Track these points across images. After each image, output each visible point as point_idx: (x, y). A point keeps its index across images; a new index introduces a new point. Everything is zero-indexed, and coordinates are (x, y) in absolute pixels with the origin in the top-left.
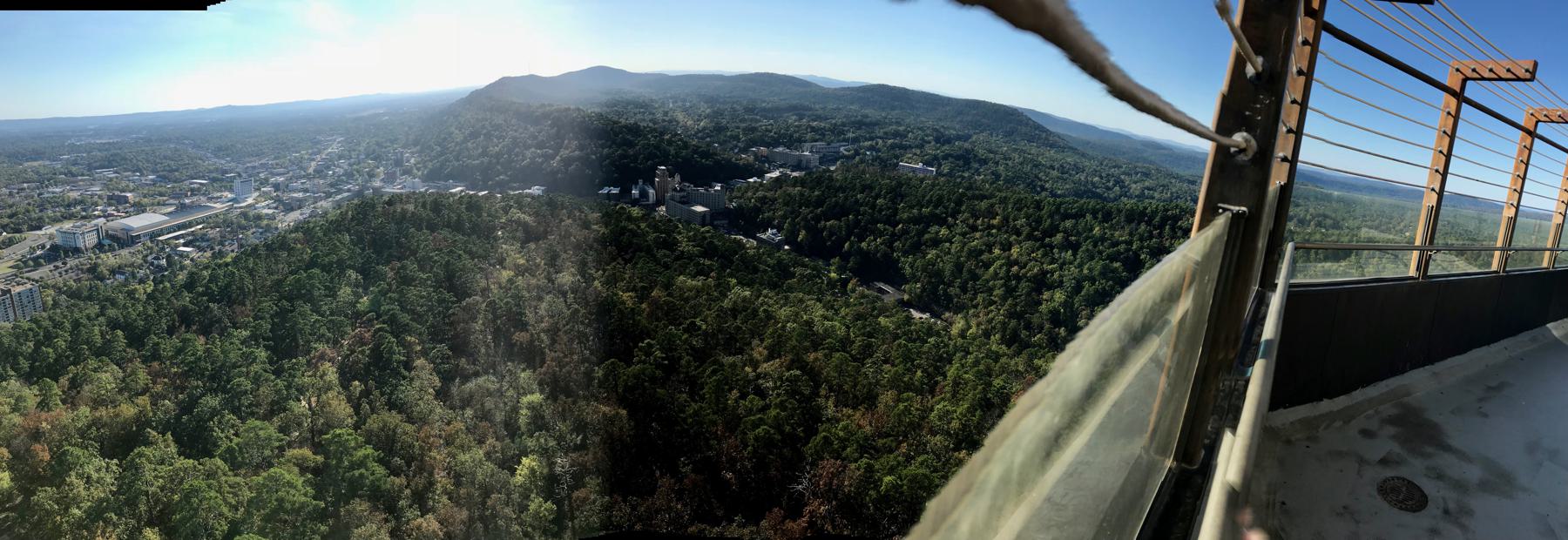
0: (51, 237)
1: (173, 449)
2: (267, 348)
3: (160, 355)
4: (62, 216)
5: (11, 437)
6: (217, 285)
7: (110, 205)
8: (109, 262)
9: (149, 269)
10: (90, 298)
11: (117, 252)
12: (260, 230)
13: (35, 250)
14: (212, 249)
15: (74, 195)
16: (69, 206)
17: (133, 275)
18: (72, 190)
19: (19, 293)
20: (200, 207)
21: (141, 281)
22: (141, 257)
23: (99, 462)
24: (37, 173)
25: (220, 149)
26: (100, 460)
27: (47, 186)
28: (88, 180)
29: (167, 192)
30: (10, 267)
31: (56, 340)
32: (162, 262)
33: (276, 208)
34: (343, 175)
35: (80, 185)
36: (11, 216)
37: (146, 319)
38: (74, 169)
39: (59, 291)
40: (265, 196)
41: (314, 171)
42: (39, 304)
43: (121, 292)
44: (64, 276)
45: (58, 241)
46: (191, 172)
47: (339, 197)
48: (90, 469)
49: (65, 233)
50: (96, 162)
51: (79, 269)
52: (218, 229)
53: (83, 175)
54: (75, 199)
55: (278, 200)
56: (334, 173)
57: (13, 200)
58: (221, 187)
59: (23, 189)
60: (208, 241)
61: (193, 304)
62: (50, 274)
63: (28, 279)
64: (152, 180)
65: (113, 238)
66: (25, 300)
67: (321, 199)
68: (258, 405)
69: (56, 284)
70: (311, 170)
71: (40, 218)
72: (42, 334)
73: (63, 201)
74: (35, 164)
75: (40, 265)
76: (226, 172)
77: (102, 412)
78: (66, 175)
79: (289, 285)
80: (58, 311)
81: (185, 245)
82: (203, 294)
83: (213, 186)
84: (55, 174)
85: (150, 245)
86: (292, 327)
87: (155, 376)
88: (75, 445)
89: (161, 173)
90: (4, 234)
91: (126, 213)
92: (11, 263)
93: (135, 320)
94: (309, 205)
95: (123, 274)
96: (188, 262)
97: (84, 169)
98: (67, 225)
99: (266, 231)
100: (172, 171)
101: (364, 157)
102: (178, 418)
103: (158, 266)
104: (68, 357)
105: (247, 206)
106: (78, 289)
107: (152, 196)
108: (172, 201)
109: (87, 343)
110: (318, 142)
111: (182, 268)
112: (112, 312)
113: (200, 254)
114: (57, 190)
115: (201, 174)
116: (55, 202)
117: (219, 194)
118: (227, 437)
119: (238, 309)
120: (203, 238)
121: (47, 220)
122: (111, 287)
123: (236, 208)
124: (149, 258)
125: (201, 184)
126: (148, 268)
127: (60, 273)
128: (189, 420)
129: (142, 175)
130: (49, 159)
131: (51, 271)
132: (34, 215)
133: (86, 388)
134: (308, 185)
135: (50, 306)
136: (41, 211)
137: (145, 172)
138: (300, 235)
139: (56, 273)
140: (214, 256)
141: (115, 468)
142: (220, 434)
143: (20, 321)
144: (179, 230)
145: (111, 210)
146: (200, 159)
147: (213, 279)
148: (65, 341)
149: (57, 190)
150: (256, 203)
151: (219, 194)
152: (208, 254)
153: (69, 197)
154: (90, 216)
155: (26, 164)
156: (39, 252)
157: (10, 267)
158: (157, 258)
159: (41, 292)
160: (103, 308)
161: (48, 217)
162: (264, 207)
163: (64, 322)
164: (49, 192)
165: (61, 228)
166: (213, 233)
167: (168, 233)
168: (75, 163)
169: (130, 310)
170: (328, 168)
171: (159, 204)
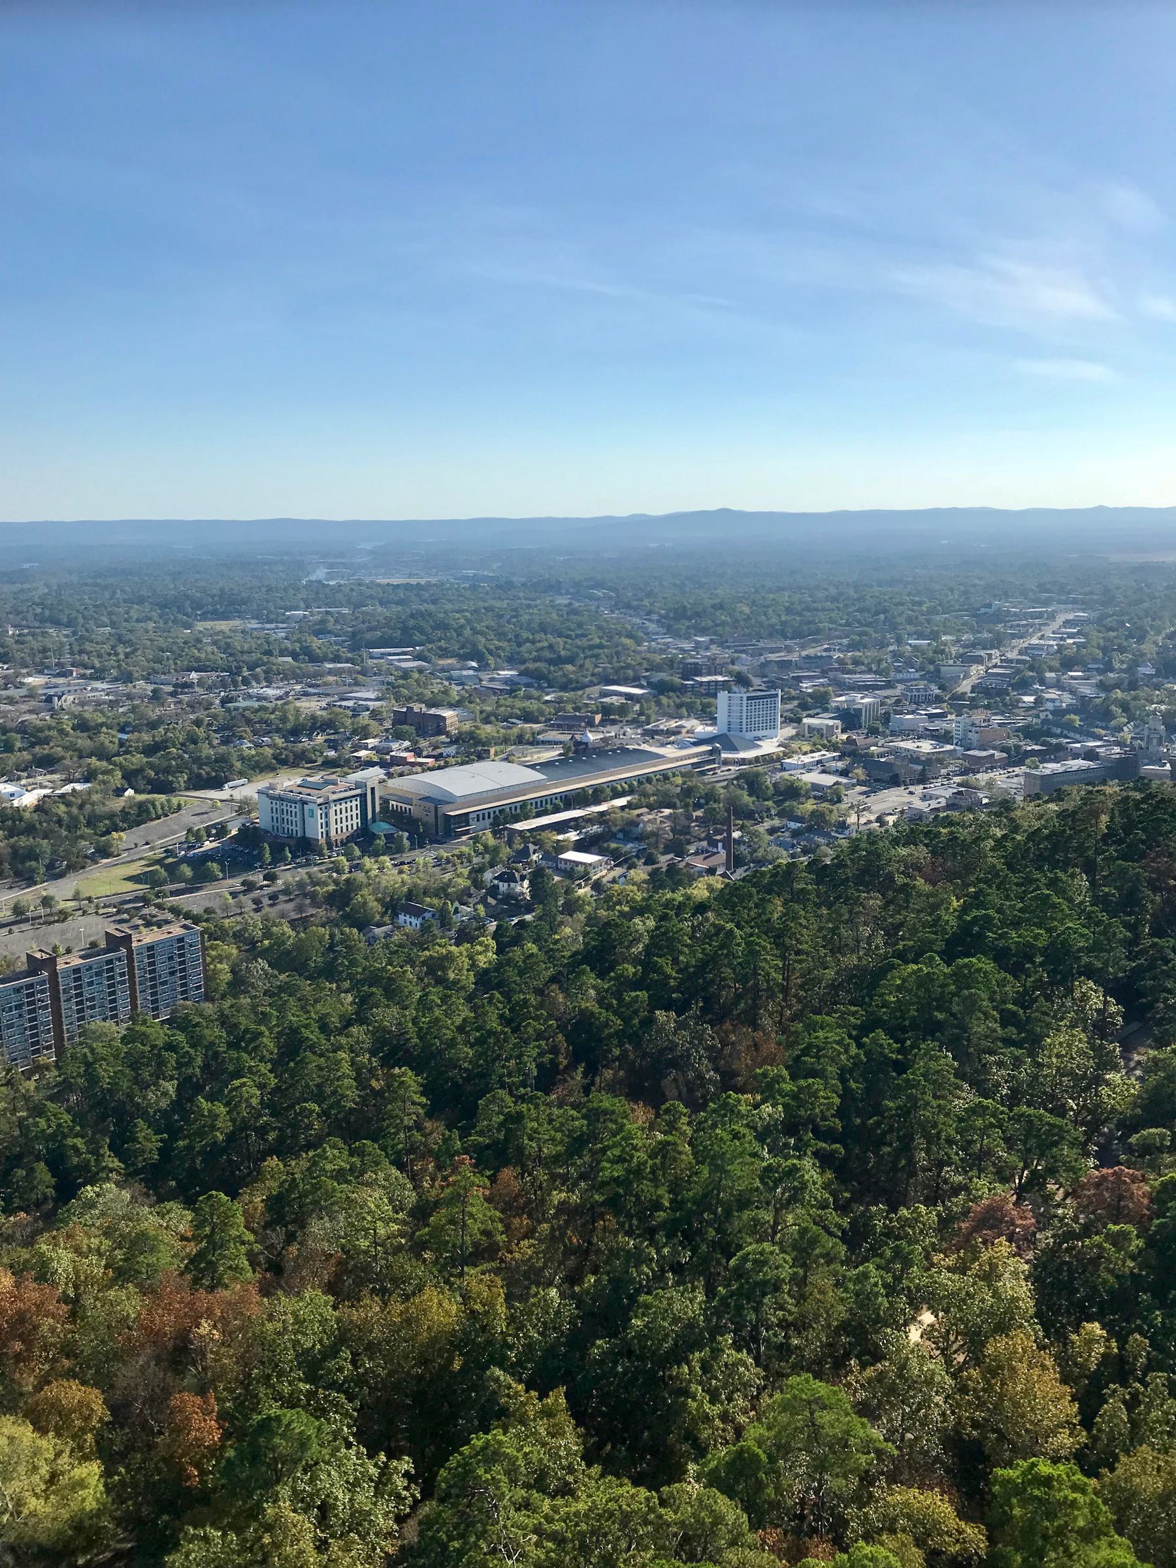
0: (243, 807)
1: (570, 1442)
2: (824, 1160)
3: (521, 1149)
4: (275, 757)
5: (116, 1356)
6: (675, 961)
7: (399, 736)
8: (385, 880)
9: (486, 905)
10: (329, 972)
11: (407, 856)
12: (794, 825)
13: (199, 839)
14: (650, 861)
15: (312, 706)
16: (296, 732)
17: (444, 919)
18: (306, 694)
19: (150, 948)
20: (625, 754)
21: (464, 936)
22: (466, 872)
23: (353, 1457)
24: (227, 648)
25: (680, 613)
26: (359, 1455)
27: (246, 682)
28: (350, 671)
29: (542, 713)
30: (130, 879)
31: (236, 1083)
32: (518, 889)
33: (844, 773)
34: (1071, 710)
35: (325, 684)
36: (150, 750)
37: (480, 1041)
38: (316, 643)
39: (251, 948)
40: (819, 739)
41: (974, 689)
42: (196, 979)
43: (410, 961)
44: (267, 909)
45: (261, 818)
46: (604, 666)
47: (1051, 767)
48: (332, 1483)
49: (280, 798)
50: (370, 629)
51: (305, 895)
52: (667, 812)
53: (337, 659)
54: (313, 718)
55: (850, 752)
56: (1039, 701)
57: (158, 711)
58: (679, 706)
59: (189, 685)
60: (640, 838)
61: (608, 1007)
62: (231, 901)
63: (175, 911)
64: (506, 681)
65: (400, 819)
66: (162, 968)
67: (991, 764)
68: (800, 1325)
69: (245, 929)
70: (965, 687)
71: (222, 759)
72: (199, 1061)
73: (284, 719)
74: (223, 626)
75: (209, 878)
76: (697, 670)
77: (370, 1309)
78: (294, 654)
79: (899, 988)
80: (245, 1001)
81: (580, 847)
82: (637, 984)
83: (658, 703)
84: (269, 653)
85: (492, 842)
86: (905, 1112)
87: (509, 1206)
88: (291, 1403)
89: (531, 666)
90: (130, 792)
91: (437, 757)
92: (135, 869)
93: (452, 1043)
94: (947, 777)
95: (417, 913)
96: (584, 891)
97: (341, 644)
98: (288, 781)
99: (810, 829)
100: (559, 661)
101: (1149, 670)
102: (578, 1340)
103: (510, 897)
104: (262, 1131)
105: (757, 759)
106: (299, 946)
107: (506, 720)
108: (553, 735)
109: (319, 1098)
110: (999, 617)
111: (572, 907)
112: (387, 1015)
113: (619, 871)
114: (270, 692)
115: (630, 673)
116: (260, 722)
117: (673, 724)
118: (725, 1417)
119: (741, 1037)
120: (629, 831)
121: (238, 765)
122: (387, 946)
123: (726, 762)
124: (488, 876)
125: (629, 697)
126: (483, 901)
127: (257, 902)
128: (613, 1355)
129: (483, 666)
130: (257, 617)
131: (234, 895)
132: (206, 751)
133: (317, 1227)
134: (952, 723)
135: (223, 987)
136: (225, 741)
137: (491, 661)
138: (921, 853)
139: (246, 900)
140: (656, 881)
141: (400, 1482)
142: (707, 1407)
143: (144, 1022)
144: (568, 807)
145: (399, 749)
146: (630, 636)
147: (661, 942)
148: (261, 1087)
149: (270, 692)
150: (786, 755)
151: (673, 724)
152: (640, 873)
153: (297, 710)
154: (348, 761)
155: (200, 626)
156: (208, 845)
157: (130, 879)
158: (508, 877)
159: (205, 949)
160: (364, 1002)
161: (242, 759)
162: (807, 768)
163: (261, 1034)
164: (250, 697)
165: (272, 787)
166: (656, 820)
167: (538, 815)
168: (320, 630)
169: (437, 1012)
170: (1023, 686)
171: (520, 740)
